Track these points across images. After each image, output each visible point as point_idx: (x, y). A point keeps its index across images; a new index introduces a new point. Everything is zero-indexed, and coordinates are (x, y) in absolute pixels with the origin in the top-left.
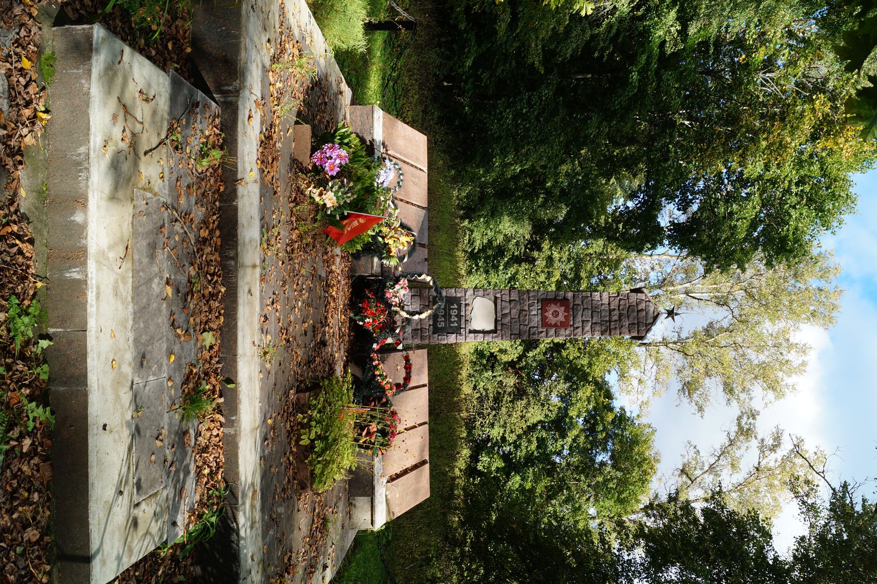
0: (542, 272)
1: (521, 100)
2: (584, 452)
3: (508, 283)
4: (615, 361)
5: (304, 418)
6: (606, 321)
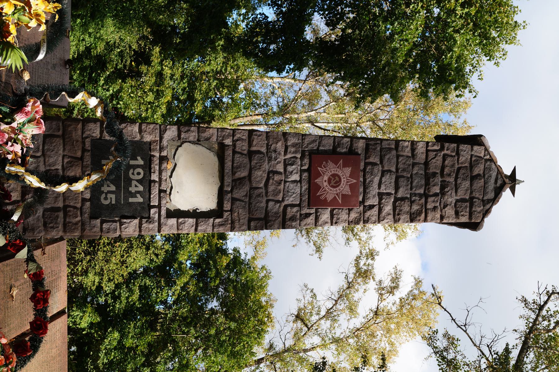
0: (151, 90)
2: (193, 301)
6: (420, 196)
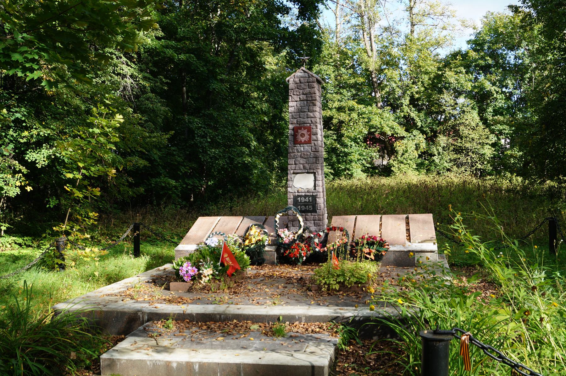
1: (200, 142)
3: (358, 144)
4: (425, 51)
5: (324, 287)
